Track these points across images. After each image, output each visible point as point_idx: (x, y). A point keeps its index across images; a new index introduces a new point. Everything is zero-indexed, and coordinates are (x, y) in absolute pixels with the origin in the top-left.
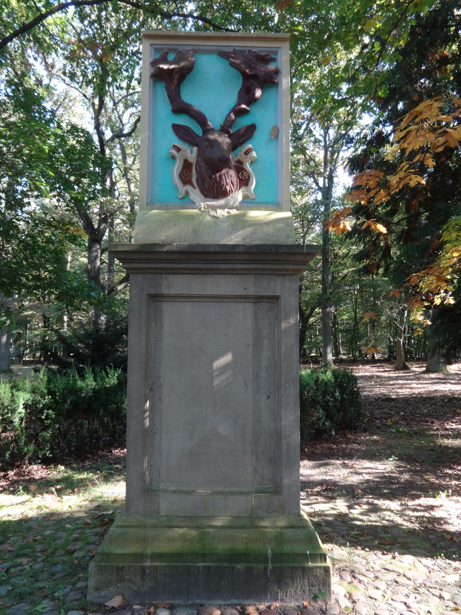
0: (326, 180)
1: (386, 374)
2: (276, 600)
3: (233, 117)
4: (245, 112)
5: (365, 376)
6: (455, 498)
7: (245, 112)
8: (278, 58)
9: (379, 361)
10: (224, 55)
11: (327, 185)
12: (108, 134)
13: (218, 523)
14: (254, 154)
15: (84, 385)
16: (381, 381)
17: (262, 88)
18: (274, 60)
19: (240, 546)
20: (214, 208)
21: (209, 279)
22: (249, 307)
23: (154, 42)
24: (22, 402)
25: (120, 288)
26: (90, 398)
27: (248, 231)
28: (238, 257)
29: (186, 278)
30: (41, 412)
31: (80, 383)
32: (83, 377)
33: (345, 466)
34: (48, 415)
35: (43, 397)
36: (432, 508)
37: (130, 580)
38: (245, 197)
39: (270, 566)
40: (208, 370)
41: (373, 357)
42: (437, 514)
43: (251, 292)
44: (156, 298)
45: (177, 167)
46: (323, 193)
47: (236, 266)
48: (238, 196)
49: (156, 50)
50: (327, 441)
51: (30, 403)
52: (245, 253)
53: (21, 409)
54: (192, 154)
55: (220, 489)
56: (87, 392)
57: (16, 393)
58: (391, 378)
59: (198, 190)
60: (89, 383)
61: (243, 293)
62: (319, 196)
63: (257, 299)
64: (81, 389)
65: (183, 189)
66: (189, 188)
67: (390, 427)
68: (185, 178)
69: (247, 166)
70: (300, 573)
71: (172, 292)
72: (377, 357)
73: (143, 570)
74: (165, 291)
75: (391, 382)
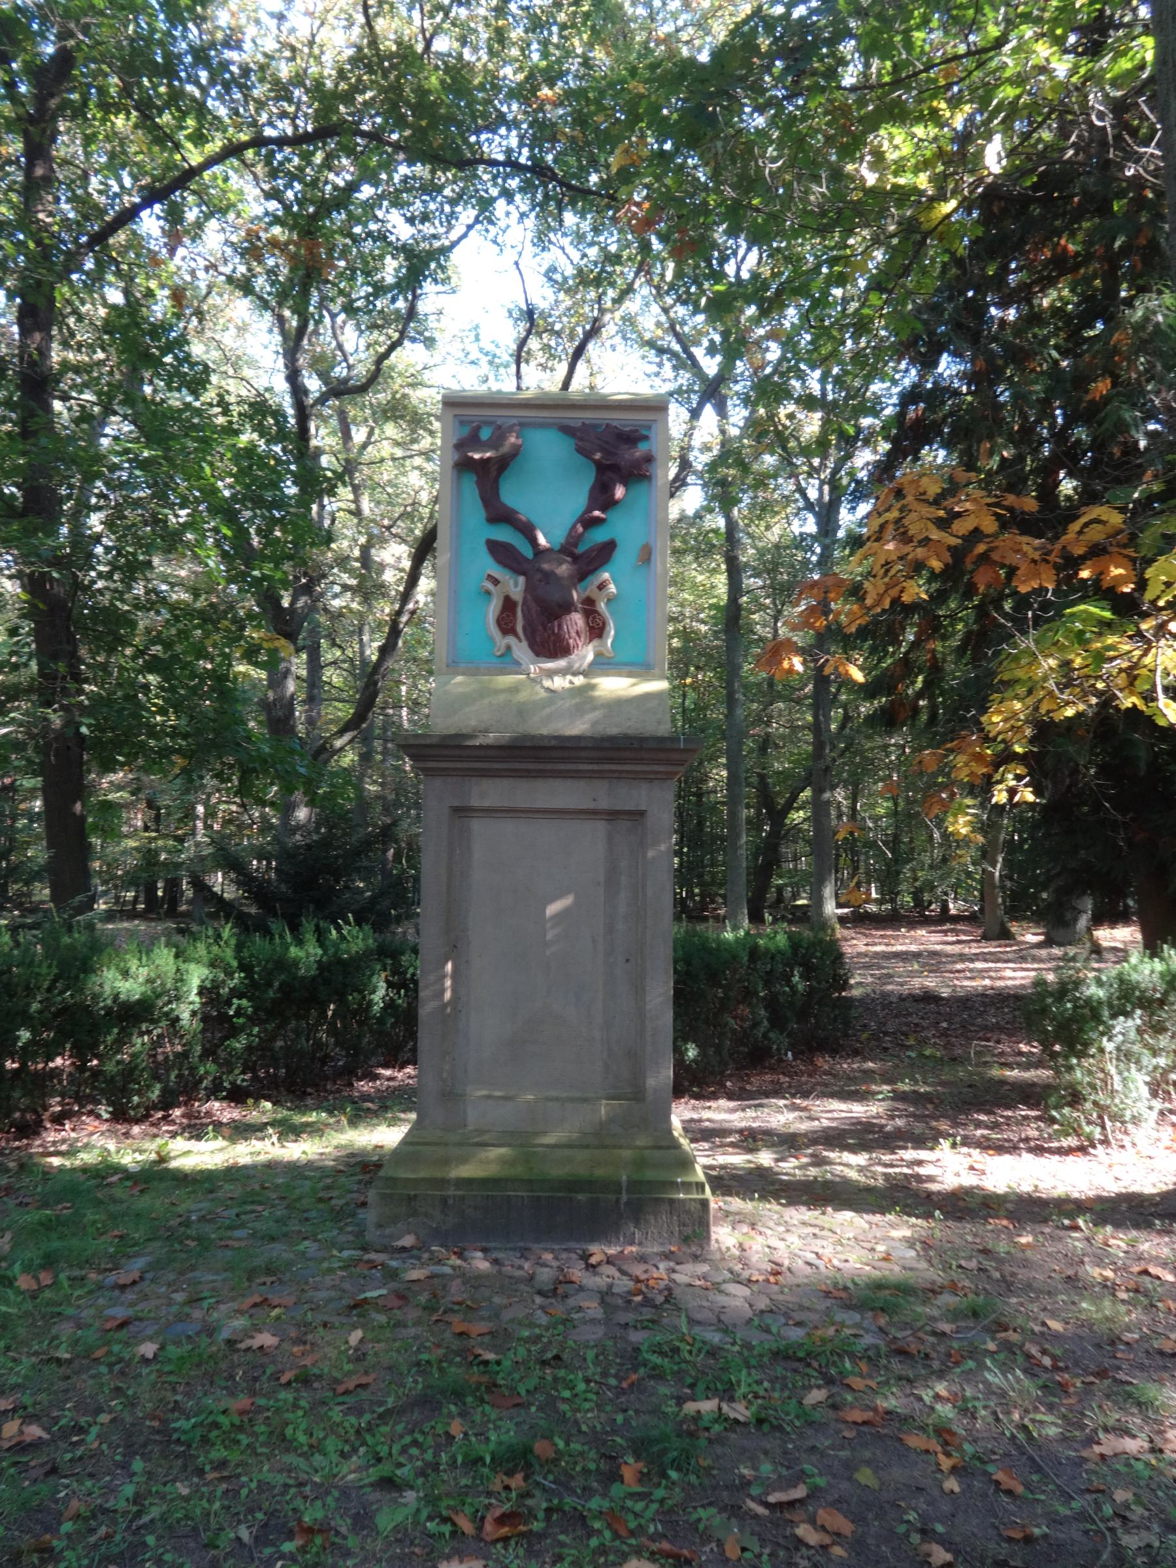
0: (826, 488)
1: (957, 949)
2: (632, 1243)
3: (580, 529)
4: (599, 521)
5: (906, 953)
6: (965, 1150)
7: (599, 521)
8: (652, 435)
9: (956, 919)
10: (566, 430)
11: (827, 498)
12: (313, 384)
13: (549, 1139)
14: (612, 588)
15: (302, 954)
16: (933, 961)
17: (626, 484)
18: (646, 438)
19: (582, 1172)
20: (551, 674)
21: (540, 784)
22: (601, 826)
23: (458, 411)
24: (195, 983)
25: (338, 743)
26: (314, 979)
27: (597, 714)
28: (583, 754)
29: (506, 783)
30: (229, 1003)
31: (294, 951)
32: (300, 943)
33: (794, 1108)
34: (239, 1007)
35: (230, 974)
36: (920, 1163)
37: (426, 1215)
38: (598, 655)
39: (624, 1197)
40: (539, 940)
41: (945, 908)
42: (922, 1171)
43: (604, 804)
44: (461, 812)
45: (494, 608)
46: (817, 515)
47: (581, 767)
48: (586, 654)
49: (462, 423)
50: (773, 1069)
51: (208, 984)
52: (593, 748)
53: (193, 997)
54: (516, 587)
55: (553, 1093)
56: (308, 969)
57: (183, 967)
58: (962, 957)
59: (525, 644)
60: (306, 954)
61: (592, 805)
62: (810, 526)
63: (613, 815)
64: (296, 963)
65: (503, 641)
66: (511, 640)
67: (909, 1048)
68: (505, 625)
69: (602, 606)
70: (665, 1207)
71: (486, 803)
72: (953, 909)
73: (444, 1200)
74: (475, 802)
75: (959, 966)
